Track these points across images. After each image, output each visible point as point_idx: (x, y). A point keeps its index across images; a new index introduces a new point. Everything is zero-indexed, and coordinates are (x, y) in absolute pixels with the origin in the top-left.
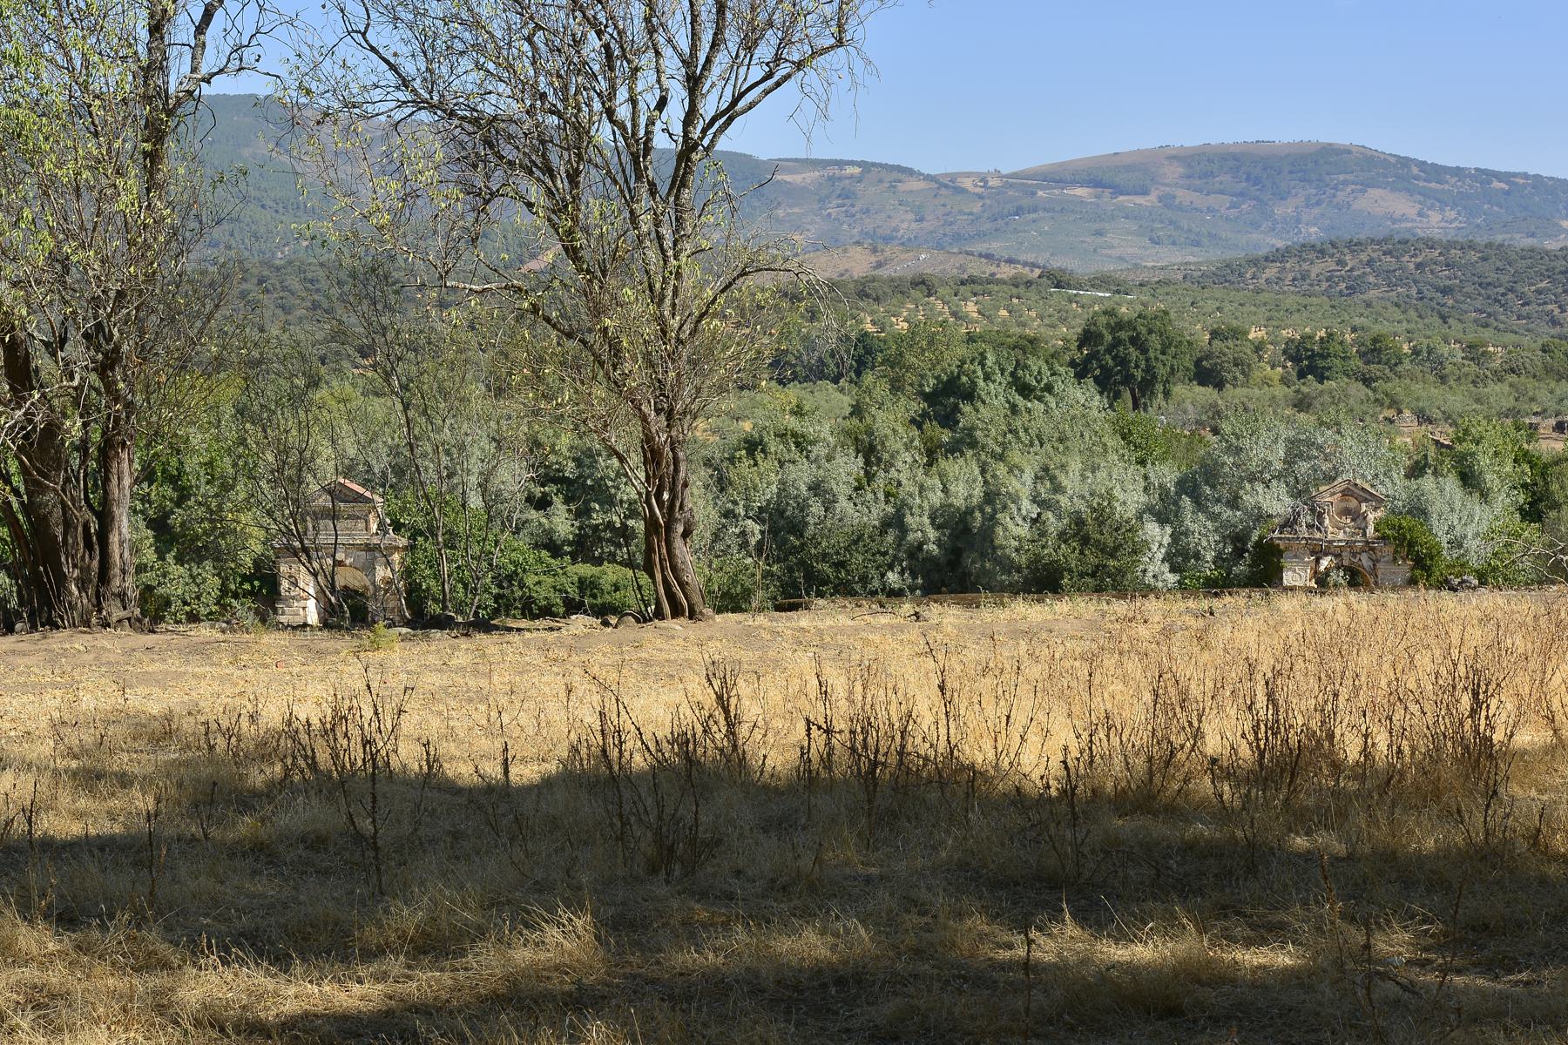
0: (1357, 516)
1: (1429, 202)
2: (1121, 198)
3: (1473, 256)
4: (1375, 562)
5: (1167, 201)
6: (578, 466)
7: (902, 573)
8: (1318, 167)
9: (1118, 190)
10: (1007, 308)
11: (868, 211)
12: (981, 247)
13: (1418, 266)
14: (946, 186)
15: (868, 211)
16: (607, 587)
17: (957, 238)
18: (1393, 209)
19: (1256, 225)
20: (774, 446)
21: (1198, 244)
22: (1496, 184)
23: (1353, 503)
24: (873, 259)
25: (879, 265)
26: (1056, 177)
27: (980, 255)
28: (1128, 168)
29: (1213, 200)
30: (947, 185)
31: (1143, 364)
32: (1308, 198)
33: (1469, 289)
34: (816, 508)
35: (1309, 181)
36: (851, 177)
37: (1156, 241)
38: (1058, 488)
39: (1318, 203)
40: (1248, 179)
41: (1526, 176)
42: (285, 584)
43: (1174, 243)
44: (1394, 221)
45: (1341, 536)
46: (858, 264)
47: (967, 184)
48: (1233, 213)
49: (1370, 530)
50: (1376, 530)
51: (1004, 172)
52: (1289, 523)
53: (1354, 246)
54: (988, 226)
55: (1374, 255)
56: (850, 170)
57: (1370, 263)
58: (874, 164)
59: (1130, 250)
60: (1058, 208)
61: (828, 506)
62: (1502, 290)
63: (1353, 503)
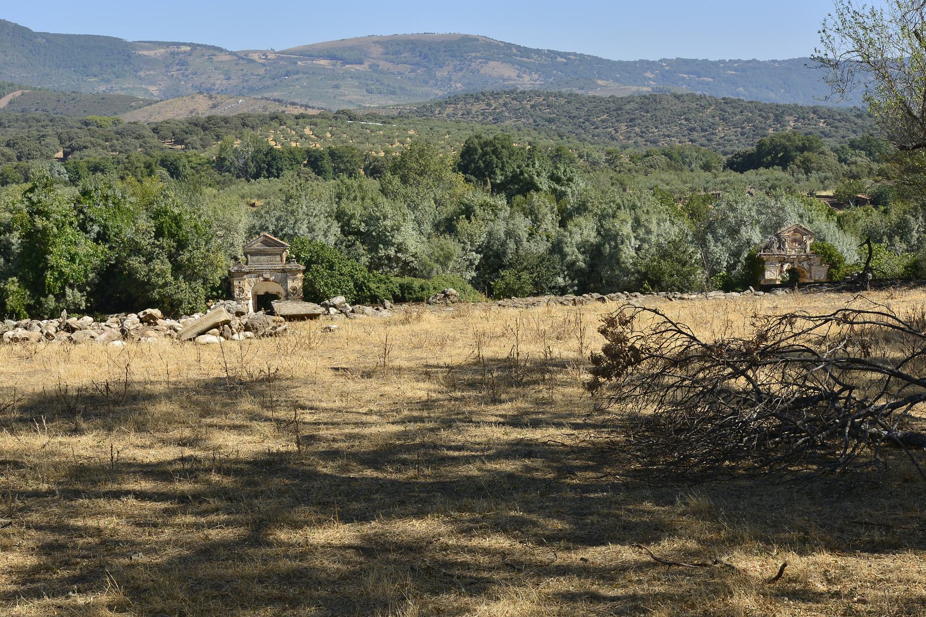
0: (801, 242)
1: (523, 69)
2: (347, 66)
4: (810, 265)
6: (366, 225)
7: (564, 278)
8: (461, 48)
9: (345, 62)
10: (331, 132)
11: (196, 73)
12: (276, 95)
13: (532, 106)
14: (243, 59)
15: (196, 73)
16: (417, 289)
17: (251, 90)
18: (502, 73)
21: (394, 93)
22: (559, 59)
23: (798, 236)
25: (214, 106)
26: (308, 53)
27: (275, 100)
28: (351, 48)
29: (401, 67)
30: (243, 58)
32: (455, 66)
33: (564, 120)
34: (511, 245)
35: (455, 57)
36: (185, 52)
37: (370, 92)
38: (649, 232)
39: (461, 70)
40: (420, 56)
41: (575, 54)
42: (237, 291)
44: (504, 80)
45: (793, 253)
46: (202, 107)
47: (255, 57)
48: (413, 75)
49: (808, 250)
50: (811, 249)
51: (277, 50)
52: (767, 247)
53: (495, 95)
54: (269, 83)
55: (507, 100)
56: (183, 48)
57: (505, 105)
58: (198, 45)
59: (355, 97)
60: (311, 72)
61: (518, 242)
62: (582, 120)
63: (798, 236)
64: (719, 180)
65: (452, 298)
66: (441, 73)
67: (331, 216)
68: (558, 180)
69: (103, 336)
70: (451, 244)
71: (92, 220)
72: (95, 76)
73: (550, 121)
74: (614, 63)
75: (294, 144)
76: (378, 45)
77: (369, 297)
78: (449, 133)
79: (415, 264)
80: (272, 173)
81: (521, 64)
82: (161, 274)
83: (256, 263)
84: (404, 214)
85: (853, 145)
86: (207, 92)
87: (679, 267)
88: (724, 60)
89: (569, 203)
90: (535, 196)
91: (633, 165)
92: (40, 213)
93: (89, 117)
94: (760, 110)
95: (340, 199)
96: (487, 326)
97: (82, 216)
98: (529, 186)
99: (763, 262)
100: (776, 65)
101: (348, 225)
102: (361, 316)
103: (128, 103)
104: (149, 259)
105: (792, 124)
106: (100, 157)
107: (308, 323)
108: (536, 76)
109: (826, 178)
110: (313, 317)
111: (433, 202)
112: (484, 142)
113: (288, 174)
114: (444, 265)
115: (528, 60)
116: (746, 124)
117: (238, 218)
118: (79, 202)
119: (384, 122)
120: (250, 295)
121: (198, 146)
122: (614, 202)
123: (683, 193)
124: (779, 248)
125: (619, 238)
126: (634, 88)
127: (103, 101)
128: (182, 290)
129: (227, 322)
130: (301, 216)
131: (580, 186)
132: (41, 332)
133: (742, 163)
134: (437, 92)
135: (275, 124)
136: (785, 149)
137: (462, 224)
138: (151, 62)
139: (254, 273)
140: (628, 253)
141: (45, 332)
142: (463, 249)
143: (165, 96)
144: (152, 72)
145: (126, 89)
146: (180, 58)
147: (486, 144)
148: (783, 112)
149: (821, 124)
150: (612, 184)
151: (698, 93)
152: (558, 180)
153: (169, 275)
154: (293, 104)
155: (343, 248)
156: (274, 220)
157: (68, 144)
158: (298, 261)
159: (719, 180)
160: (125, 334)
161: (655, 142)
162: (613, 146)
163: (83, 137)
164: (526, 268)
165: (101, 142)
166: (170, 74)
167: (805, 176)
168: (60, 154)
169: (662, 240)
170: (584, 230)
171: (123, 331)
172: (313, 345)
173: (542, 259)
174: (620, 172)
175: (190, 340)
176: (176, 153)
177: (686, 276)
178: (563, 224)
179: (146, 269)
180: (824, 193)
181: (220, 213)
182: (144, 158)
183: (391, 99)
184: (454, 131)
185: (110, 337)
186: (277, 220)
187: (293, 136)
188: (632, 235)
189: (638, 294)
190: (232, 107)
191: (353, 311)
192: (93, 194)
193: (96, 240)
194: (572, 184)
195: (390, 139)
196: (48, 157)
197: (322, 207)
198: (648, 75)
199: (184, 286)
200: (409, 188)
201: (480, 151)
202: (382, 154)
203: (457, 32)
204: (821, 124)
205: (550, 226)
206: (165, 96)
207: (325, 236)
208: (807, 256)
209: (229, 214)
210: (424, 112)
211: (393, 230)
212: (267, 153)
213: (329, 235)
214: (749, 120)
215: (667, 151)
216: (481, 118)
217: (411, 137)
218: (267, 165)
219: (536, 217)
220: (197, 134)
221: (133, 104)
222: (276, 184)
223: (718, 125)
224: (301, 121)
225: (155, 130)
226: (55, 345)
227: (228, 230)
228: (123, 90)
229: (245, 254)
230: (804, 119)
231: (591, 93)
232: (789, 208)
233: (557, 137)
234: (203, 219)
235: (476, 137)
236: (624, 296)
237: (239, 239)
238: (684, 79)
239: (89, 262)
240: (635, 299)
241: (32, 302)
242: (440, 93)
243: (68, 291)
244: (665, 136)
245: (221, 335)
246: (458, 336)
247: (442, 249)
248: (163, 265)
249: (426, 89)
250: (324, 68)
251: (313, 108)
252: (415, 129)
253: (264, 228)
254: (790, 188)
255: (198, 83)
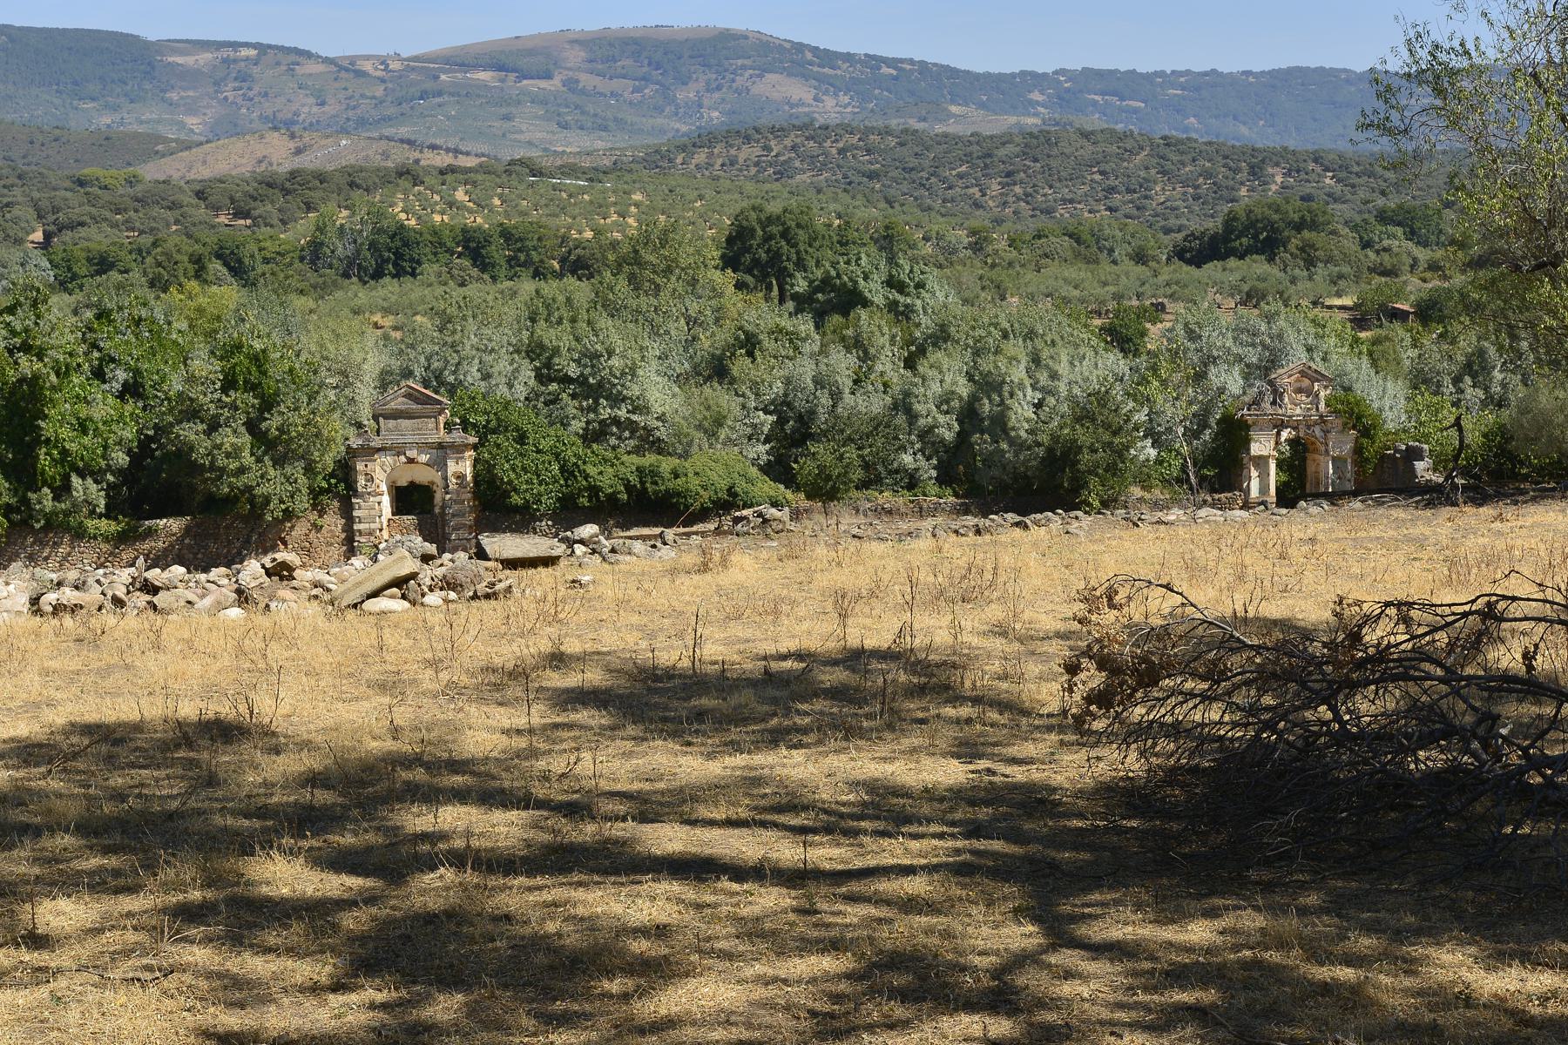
1: (824, 87)
2: (525, 82)
3: (892, 141)
4: (1326, 432)
5: (570, 84)
8: (717, 52)
10: (500, 197)
11: (266, 94)
12: (404, 131)
13: (841, 151)
14: (347, 70)
15: (266, 94)
17: (362, 122)
18: (787, 92)
19: (659, 110)
20: (768, 343)
21: (605, 129)
22: (885, 70)
24: (292, 145)
25: (298, 151)
26: (459, 60)
27: (402, 141)
28: (531, 52)
29: (616, 84)
30: (346, 68)
31: (794, 257)
32: (708, 83)
36: (247, 59)
37: (564, 126)
38: (1054, 376)
39: (719, 88)
40: (650, 64)
41: (911, 62)
42: (361, 481)
43: (582, 128)
44: (792, 106)
45: (1298, 411)
46: (279, 154)
47: (368, 67)
49: (1322, 406)
50: (1327, 405)
51: (404, 55)
52: (1256, 402)
53: (778, 132)
54: (392, 111)
55: (798, 140)
56: (244, 52)
57: (794, 148)
58: (270, 46)
59: (539, 135)
61: (836, 396)
64: (1162, 279)
65: (774, 524)
66: (685, 94)
67: (518, 351)
68: (901, 287)
69: (207, 601)
70: (719, 396)
71: (113, 360)
72: (93, 99)
73: (872, 176)
74: (977, 76)
75: (437, 218)
76: (577, 47)
77: (586, 489)
78: (701, 198)
79: (662, 433)
80: (403, 268)
81: (820, 79)
82: (235, 453)
83: (393, 431)
84: (642, 348)
85: (1383, 217)
86: (286, 126)
87: (1106, 437)
88: (1163, 72)
89: (918, 325)
90: (863, 314)
91: (1015, 253)
92: (26, 348)
93: (86, 171)
94: (1226, 157)
95: (533, 320)
96: (843, 578)
97: (96, 354)
98: (850, 300)
99: (1248, 427)
100: (1251, 79)
101: (548, 365)
102: (628, 558)
103: (151, 146)
104: (213, 426)
105: (1279, 179)
106: (108, 241)
107: (543, 572)
108: (846, 99)
109: (1341, 276)
110: (549, 561)
111: (682, 321)
112: (768, 218)
113: (430, 269)
114: (712, 435)
115: (831, 72)
116: (1201, 180)
117: (362, 355)
118: (91, 330)
119: (591, 180)
120: (384, 488)
121: (275, 221)
122: (996, 325)
123: (1103, 302)
124: (1274, 403)
125: (1006, 388)
126: (1013, 120)
127: (107, 142)
128: (273, 483)
129: (413, 576)
130: (467, 350)
131: (938, 297)
132: (103, 593)
133: (1203, 251)
134: (677, 126)
135: (404, 183)
136: (1272, 227)
137: (740, 366)
138: (191, 77)
139: (390, 449)
140: (1021, 413)
141: (109, 594)
142: (744, 407)
143: (217, 132)
144: (191, 93)
145: (147, 122)
146: (242, 70)
147: (770, 220)
148: (1263, 161)
149: (1328, 181)
150: (983, 288)
151: (1120, 127)
152: (901, 287)
153: (246, 453)
154: (433, 147)
155: (540, 405)
156: (422, 359)
157: (51, 218)
158: (465, 430)
159: (1162, 279)
160: (243, 597)
161: (1048, 212)
162: (979, 220)
163: (76, 206)
164: (850, 439)
165: (108, 214)
166: (221, 96)
167: (1305, 273)
168: (38, 236)
169: (1076, 391)
170: (947, 375)
171: (239, 592)
172: (561, 616)
173: (877, 424)
174: (993, 266)
175: (355, 606)
176: (237, 234)
177: (1121, 452)
178: (910, 363)
179: (208, 444)
180: (1338, 302)
181: (331, 348)
182: (190, 247)
183: (600, 138)
184: (709, 193)
185: (219, 603)
186: (428, 359)
187: (436, 203)
188: (1027, 382)
189: (1079, 513)
190: (333, 152)
191: (613, 551)
192: (114, 316)
193: (121, 396)
194: (924, 293)
195: (601, 208)
196: (19, 242)
197: (503, 337)
198: (1036, 96)
199: (272, 472)
200: (643, 298)
201: (760, 232)
202: (589, 234)
203: (711, 25)
204: (1328, 181)
205: (889, 366)
206: (217, 132)
207: (510, 386)
208: (1321, 416)
209: (349, 347)
210: (658, 161)
211: (623, 374)
212: (395, 234)
213: (515, 382)
214: (1207, 174)
215: (1071, 228)
216: (753, 170)
217: (637, 205)
218: (392, 256)
219: (866, 352)
220: (272, 202)
221: (160, 147)
222: (411, 290)
223: (1155, 183)
224: (449, 178)
225: (200, 195)
226: (131, 621)
227: (344, 374)
228: (142, 122)
229: (375, 418)
230: (1298, 171)
231: (939, 129)
232: (1291, 335)
233: (883, 205)
234: (303, 358)
235: (754, 208)
236: (1056, 518)
237: (366, 393)
238: (1095, 103)
239: (110, 431)
240: (1075, 524)
241: (13, 501)
242: (684, 128)
243: (76, 480)
244: (1065, 201)
245: (404, 597)
246: (798, 596)
247: (708, 408)
248: (234, 437)
249: (660, 121)
250: (485, 86)
251: (468, 154)
252: (643, 190)
253: (408, 374)
254: (1281, 293)
255: (269, 112)
